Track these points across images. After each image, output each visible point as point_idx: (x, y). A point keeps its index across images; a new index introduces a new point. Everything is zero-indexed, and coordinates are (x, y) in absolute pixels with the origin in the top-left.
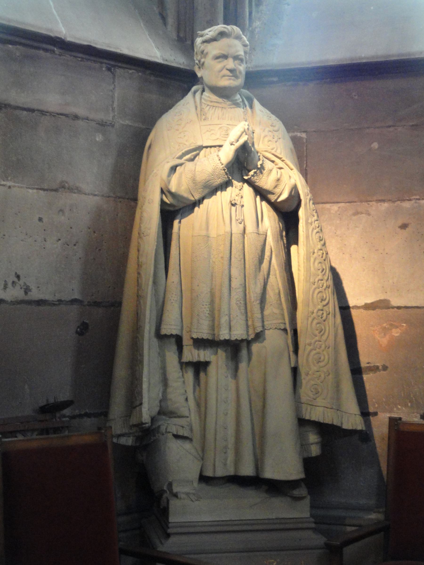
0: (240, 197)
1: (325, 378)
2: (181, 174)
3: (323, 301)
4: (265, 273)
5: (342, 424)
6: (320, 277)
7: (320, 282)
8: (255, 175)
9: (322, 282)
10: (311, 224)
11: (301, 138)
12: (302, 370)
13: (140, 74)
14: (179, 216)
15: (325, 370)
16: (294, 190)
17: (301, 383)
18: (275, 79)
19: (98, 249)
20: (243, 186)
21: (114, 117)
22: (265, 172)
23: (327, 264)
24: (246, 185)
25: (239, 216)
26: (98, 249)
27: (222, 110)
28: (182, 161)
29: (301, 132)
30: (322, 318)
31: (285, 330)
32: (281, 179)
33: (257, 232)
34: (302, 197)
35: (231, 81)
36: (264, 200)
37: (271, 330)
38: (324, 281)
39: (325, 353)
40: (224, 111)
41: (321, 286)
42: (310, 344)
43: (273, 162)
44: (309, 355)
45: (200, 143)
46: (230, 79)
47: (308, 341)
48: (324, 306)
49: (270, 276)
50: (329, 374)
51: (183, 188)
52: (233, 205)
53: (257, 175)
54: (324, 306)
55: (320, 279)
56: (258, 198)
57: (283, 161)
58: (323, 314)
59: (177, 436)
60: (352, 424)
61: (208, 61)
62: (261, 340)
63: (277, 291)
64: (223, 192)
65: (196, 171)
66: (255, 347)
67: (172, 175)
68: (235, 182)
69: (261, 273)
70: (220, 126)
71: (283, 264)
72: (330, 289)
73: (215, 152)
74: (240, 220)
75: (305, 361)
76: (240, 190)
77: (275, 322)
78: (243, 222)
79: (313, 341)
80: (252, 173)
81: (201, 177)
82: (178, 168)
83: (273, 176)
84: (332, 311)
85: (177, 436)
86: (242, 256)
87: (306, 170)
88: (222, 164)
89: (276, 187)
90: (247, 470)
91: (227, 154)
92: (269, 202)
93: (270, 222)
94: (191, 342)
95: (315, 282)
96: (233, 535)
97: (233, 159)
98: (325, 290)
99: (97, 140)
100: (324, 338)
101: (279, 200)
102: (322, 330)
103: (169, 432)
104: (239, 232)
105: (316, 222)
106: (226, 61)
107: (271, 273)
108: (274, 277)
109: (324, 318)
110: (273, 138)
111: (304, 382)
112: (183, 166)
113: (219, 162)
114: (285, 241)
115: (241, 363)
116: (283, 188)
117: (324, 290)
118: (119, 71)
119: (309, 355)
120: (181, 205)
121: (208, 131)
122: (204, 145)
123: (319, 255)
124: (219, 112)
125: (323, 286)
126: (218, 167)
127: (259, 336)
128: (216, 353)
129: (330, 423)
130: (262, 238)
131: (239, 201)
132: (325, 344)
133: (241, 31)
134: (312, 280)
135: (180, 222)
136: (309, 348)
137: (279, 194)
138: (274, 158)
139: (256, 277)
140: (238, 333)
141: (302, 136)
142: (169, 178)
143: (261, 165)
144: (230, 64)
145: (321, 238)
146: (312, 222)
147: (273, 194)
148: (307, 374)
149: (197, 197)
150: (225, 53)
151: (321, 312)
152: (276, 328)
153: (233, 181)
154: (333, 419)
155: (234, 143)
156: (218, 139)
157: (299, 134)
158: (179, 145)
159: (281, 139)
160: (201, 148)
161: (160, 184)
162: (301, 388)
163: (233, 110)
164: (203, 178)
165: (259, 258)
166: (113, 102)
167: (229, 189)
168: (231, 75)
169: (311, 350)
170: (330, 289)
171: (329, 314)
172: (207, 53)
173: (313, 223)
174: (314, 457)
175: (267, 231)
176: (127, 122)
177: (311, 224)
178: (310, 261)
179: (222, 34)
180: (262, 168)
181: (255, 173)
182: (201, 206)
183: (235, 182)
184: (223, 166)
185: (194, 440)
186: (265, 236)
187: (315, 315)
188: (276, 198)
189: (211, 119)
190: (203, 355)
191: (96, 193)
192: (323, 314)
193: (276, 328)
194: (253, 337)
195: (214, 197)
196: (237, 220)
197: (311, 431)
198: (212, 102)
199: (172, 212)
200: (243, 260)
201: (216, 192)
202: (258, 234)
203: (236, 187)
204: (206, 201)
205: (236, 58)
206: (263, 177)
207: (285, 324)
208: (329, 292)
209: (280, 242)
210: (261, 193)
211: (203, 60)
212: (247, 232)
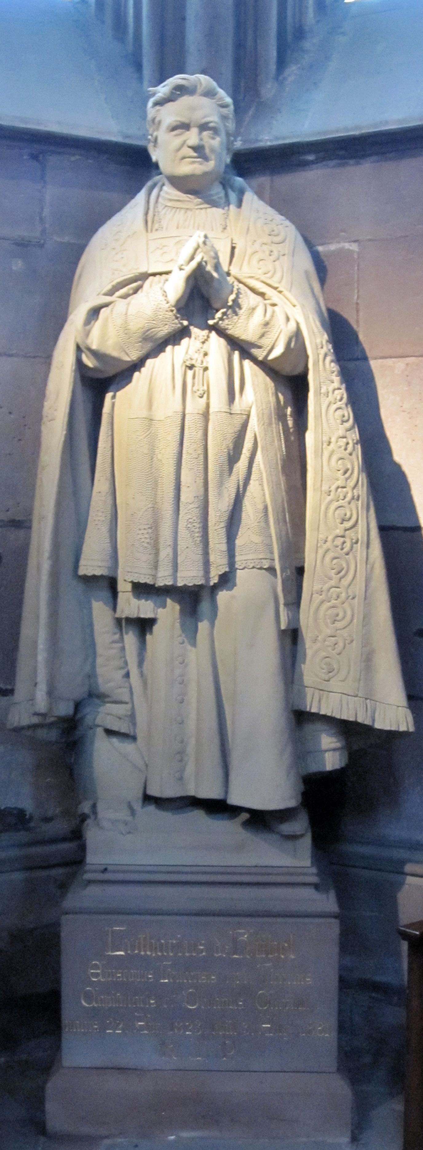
0: (202, 354)
1: (344, 648)
2: (106, 320)
3: (345, 522)
4: (240, 478)
5: (374, 720)
6: (339, 483)
7: (340, 490)
8: (225, 317)
9: (344, 490)
10: (327, 394)
11: (351, 252)
12: (307, 633)
13: (90, 161)
14: (112, 387)
15: (346, 635)
16: (294, 340)
17: (305, 655)
18: (311, 157)
19: (16, 439)
20: (208, 337)
21: (44, 231)
22: (241, 312)
23: (355, 460)
24: (213, 334)
25: (198, 385)
26: (16, 439)
27: (186, 212)
28: (108, 299)
29: (349, 242)
30: (342, 549)
31: (271, 570)
32: (272, 323)
33: (228, 411)
34: (310, 352)
35: (196, 166)
36: (247, 358)
37: (246, 570)
38: (348, 489)
39: (346, 605)
40: (189, 213)
41: (342, 497)
42: (320, 593)
43: (262, 295)
44: (317, 609)
45: (143, 269)
46: (193, 162)
47: (317, 587)
48: (346, 530)
49: (251, 482)
50: (352, 641)
51: (110, 342)
52: (191, 367)
53: (228, 318)
54: (346, 530)
55: (341, 485)
56: (236, 355)
57: (280, 292)
58: (344, 543)
59: (110, 732)
60: (391, 721)
61: (162, 134)
62: (229, 584)
63: (261, 507)
64: (176, 347)
65: (129, 313)
66: (222, 596)
67: (93, 322)
68: (194, 330)
69: (234, 477)
70: (177, 239)
71: (279, 462)
72: (360, 503)
73: (159, 282)
74: (201, 392)
75: (311, 620)
76: (203, 343)
77: (251, 557)
78: (205, 396)
79: (326, 587)
80: (219, 315)
81: (137, 325)
82: (103, 311)
83: (258, 318)
84: (362, 537)
85: (110, 732)
86: (200, 451)
87: (357, 304)
88: (168, 303)
89: (263, 335)
90: (210, 791)
91: (175, 286)
92: (254, 360)
93: (258, 393)
94: (129, 587)
95: (330, 491)
96: (205, 889)
97: (185, 292)
98: (349, 503)
99: (14, 268)
100: (345, 582)
101: (271, 357)
102: (343, 569)
103: (99, 726)
104: (196, 411)
105: (337, 392)
106: (188, 133)
107: (253, 476)
108: (257, 483)
109: (346, 550)
110: (270, 255)
111: (309, 653)
112: (110, 307)
113: (163, 298)
114: (290, 423)
115: (201, 622)
116: (275, 337)
117: (346, 504)
118: (53, 160)
119: (317, 609)
120: (110, 371)
121: (158, 248)
122: (151, 271)
123: (340, 447)
124: (180, 216)
125: (345, 497)
126: (162, 306)
127: (226, 580)
128: (164, 606)
129: (352, 719)
130: (238, 422)
131: (199, 361)
132: (347, 593)
133: (214, 80)
134: (325, 488)
135: (114, 397)
136: (317, 599)
137: (269, 348)
138: (263, 288)
139: (221, 483)
140: (189, 575)
141: (351, 248)
142: (88, 327)
143: (234, 301)
144: (193, 137)
145: (346, 418)
146: (328, 392)
147: (260, 347)
148: (315, 641)
149: (133, 356)
150: (185, 120)
151: (342, 540)
152: (253, 567)
153: (192, 328)
154: (356, 714)
155: (183, 267)
156: (172, 260)
157: (347, 246)
158: (113, 274)
159: (286, 257)
160: (144, 277)
161: (75, 338)
162: (304, 663)
163: (203, 211)
164: (141, 325)
165: (229, 454)
166: (42, 209)
167: (185, 341)
168: (195, 154)
169: (322, 602)
170: (360, 503)
171: (357, 542)
172: (160, 122)
173: (330, 394)
174: (331, 772)
175: (251, 408)
176: (66, 239)
177: (327, 394)
178: (322, 456)
179: (181, 90)
180: (236, 305)
181: (224, 314)
182: (143, 370)
183: (194, 330)
184: (169, 304)
185: (139, 740)
186: (245, 417)
187: (329, 544)
188: (265, 353)
189: (167, 229)
190: (144, 608)
191: (14, 352)
192: (344, 543)
193: (253, 567)
194: (216, 581)
195: (162, 355)
196: (195, 392)
197: (325, 730)
198: (171, 200)
199: (99, 382)
200: (202, 457)
201: (166, 346)
202: (231, 414)
203: (195, 339)
204: (149, 362)
205: (203, 127)
206: (240, 321)
207: (273, 560)
208: (357, 508)
209: (274, 426)
210: (240, 347)
211: (155, 134)
212: (211, 410)
